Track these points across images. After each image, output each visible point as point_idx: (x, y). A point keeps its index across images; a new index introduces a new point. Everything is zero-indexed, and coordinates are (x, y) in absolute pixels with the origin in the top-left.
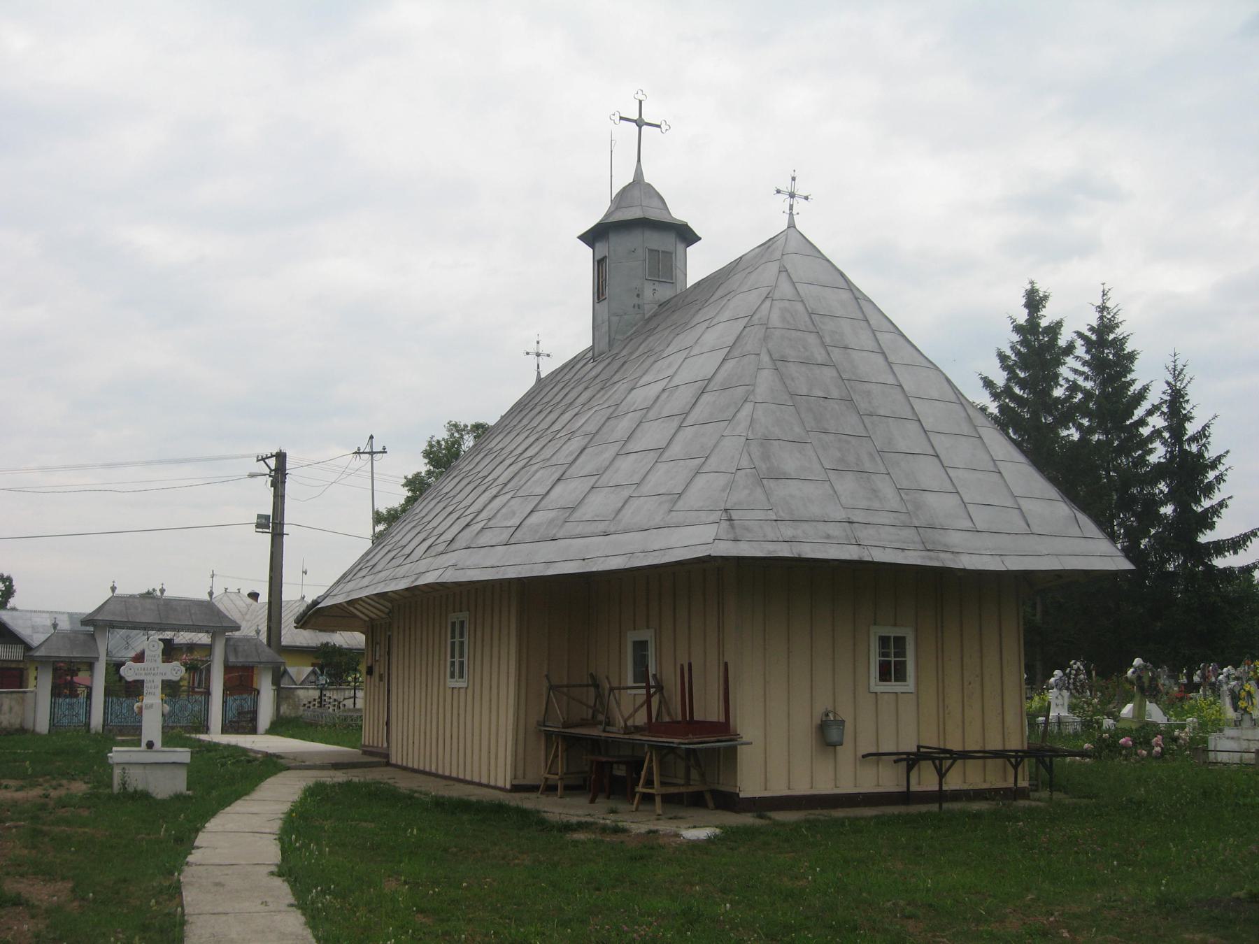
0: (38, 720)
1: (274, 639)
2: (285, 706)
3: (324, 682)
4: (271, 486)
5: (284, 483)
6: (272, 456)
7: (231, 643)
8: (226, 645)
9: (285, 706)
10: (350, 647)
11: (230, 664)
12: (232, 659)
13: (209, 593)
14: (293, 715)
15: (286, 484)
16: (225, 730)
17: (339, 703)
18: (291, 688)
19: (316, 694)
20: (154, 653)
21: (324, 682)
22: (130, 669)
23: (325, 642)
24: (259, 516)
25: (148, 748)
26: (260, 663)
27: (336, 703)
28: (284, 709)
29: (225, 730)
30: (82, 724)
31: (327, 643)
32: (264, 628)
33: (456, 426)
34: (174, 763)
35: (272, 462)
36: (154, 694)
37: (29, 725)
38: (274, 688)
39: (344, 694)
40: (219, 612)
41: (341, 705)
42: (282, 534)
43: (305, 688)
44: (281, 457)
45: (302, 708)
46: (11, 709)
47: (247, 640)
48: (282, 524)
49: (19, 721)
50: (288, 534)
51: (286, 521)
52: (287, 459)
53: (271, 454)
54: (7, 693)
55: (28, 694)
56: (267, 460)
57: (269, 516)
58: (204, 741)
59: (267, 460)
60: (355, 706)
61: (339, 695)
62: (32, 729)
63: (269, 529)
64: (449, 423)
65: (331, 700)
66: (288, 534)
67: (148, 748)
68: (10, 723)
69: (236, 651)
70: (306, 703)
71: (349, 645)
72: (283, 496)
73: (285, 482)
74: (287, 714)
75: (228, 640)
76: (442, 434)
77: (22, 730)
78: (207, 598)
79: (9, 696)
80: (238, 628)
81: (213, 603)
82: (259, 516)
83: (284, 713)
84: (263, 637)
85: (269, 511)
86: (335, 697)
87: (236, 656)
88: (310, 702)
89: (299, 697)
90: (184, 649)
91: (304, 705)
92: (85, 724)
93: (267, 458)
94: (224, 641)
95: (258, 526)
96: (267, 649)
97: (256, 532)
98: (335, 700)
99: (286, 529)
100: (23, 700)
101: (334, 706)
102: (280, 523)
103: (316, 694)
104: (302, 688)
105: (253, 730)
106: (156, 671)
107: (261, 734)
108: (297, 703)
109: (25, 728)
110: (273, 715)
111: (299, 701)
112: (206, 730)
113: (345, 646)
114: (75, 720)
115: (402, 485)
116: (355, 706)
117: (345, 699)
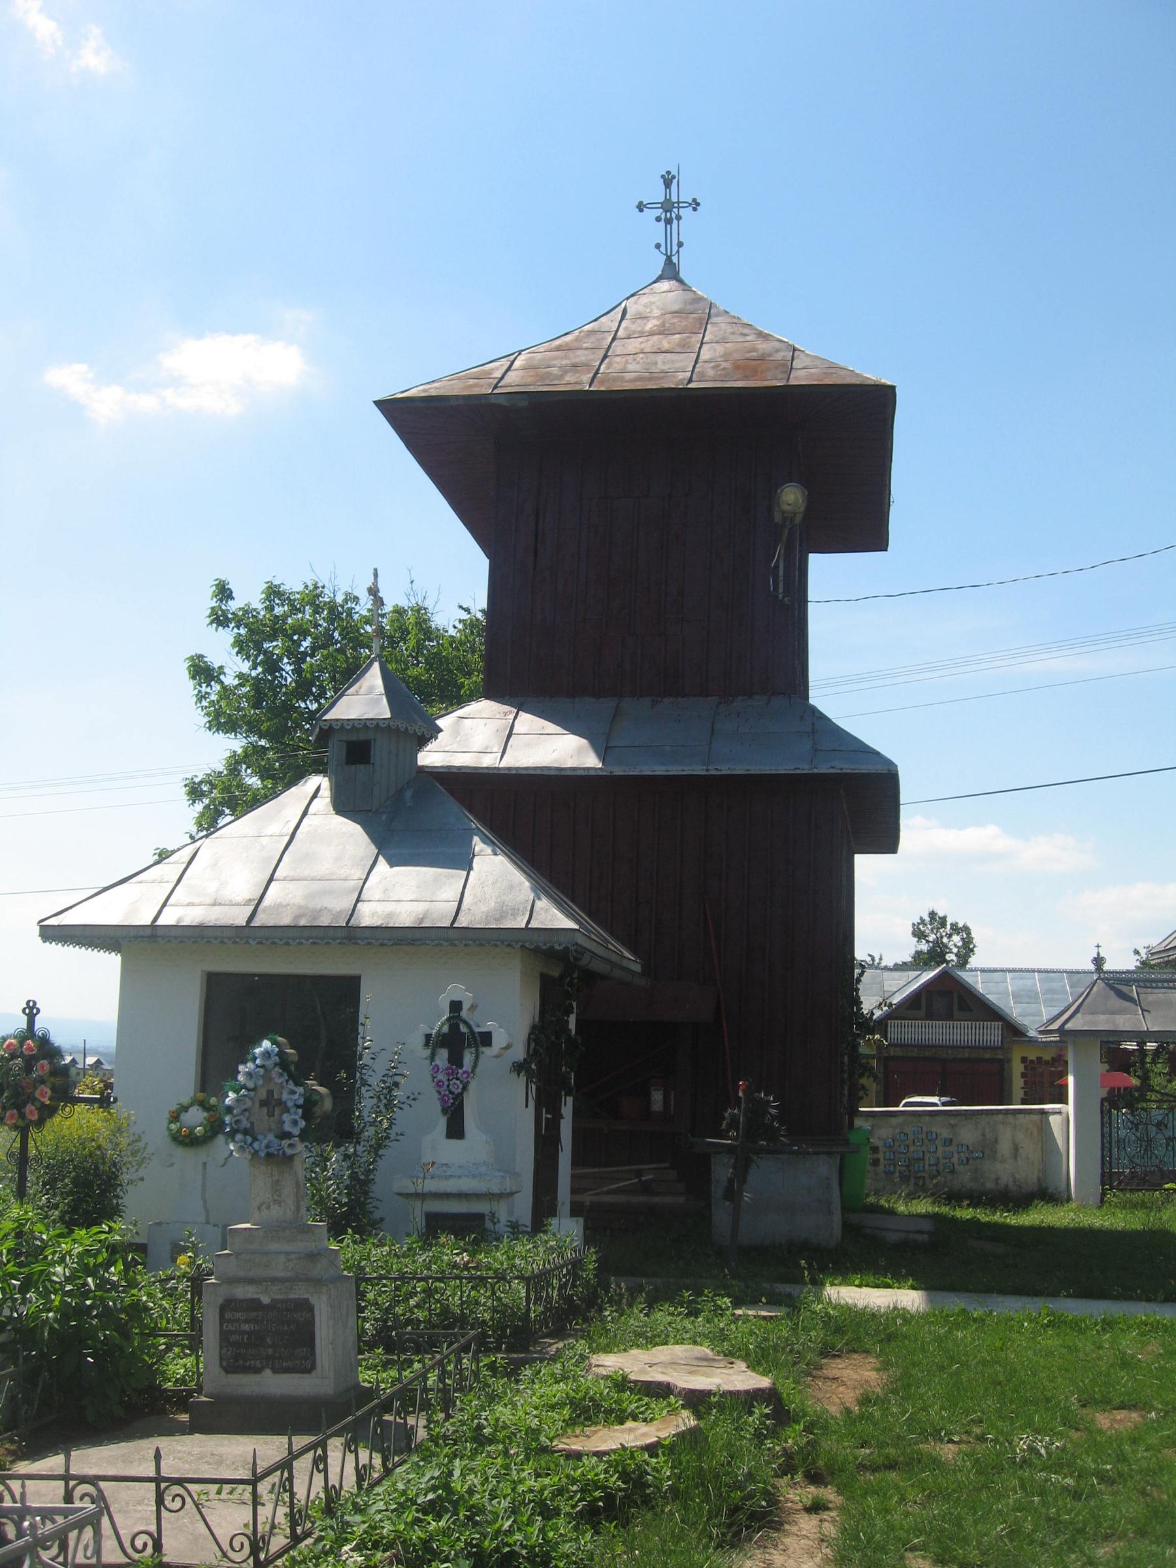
68: (1015, 1181)
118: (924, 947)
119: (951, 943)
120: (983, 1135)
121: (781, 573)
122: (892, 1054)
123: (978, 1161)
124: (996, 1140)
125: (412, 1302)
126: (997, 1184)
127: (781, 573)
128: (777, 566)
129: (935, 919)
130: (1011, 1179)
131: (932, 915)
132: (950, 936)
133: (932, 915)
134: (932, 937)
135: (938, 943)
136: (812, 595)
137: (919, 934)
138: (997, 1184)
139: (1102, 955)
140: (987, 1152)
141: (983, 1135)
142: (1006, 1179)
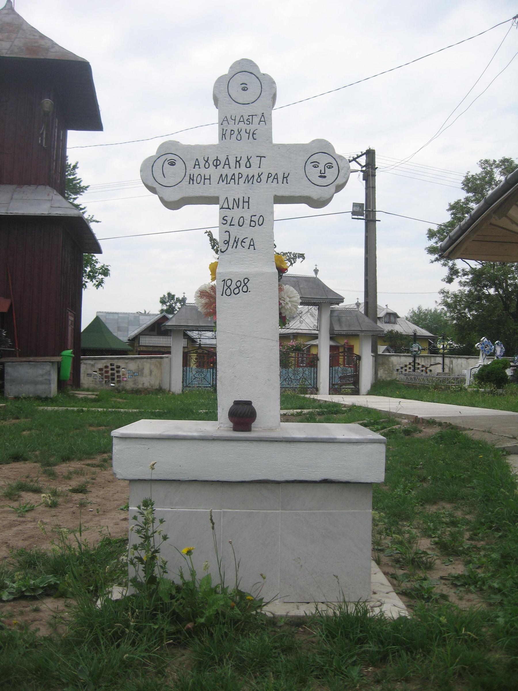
0: (173, 382)
1: (370, 311)
2: (382, 371)
3: (417, 350)
4: (363, 180)
5: (374, 175)
6: (362, 155)
7: (335, 314)
8: (331, 316)
9: (382, 371)
10: (407, 334)
11: (336, 332)
12: (337, 328)
13: (314, 270)
14: (389, 379)
15: (376, 177)
16: (334, 390)
17: (426, 368)
18: (386, 355)
19: (411, 360)
20: (246, 111)
21: (417, 350)
22: (172, 164)
23: (390, 329)
24: (355, 205)
25: (236, 428)
26: (362, 331)
27: (424, 369)
28: (381, 373)
29: (334, 390)
30: (210, 385)
31: (392, 331)
32: (362, 300)
33: (487, 161)
34: (325, 482)
35: (363, 160)
36: (252, 245)
37: (166, 386)
38: (373, 354)
39: (431, 361)
40: (324, 287)
41: (428, 371)
42: (375, 221)
43: (398, 356)
44: (370, 154)
45: (395, 373)
46: (151, 372)
47: (348, 312)
48: (374, 212)
49: (157, 383)
50: (379, 221)
51: (377, 209)
52: (376, 156)
53: (362, 152)
54: (147, 358)
55: (165, 359)
56: (357, 160)
57: (363, 204)
58: (319, 401)
59: (357, 160)
60: (443, 371)
61: (426, 362)
62: (168, 390)
63: (363, 216)
64: (480, 162)
65: (420, 366)
66: (379, 221)
67: (236, 428)
68: (150, 384)
69: (339, 321)
70: (399, 368)
71: (406, 332)
72: (374, 188)
73: (375, 176)
74: (383, 378)
75: (332, 311)
76: (477, 170)
77: (160, 390)
78: (313, 275)
79: (149, 360)
80: (341, 300)
81: (318, 279)
82: (355, 205)
83: (381, 377)
84: (362, 309)
85: (362, 200)
86: (423, 363)
87: (340, 325)
88: (402, 368)
89: (392, 363)
90: (291, 337)
91: (398, 370)
92: (213, 386)
93: (358, 157)
94: (329, 313)
95: (354, 213)
96: (366, 319)
97: (353, 218)
98: (423, 366)
99: (378, 216)
100: (161, 364)
101: (422, 371)
102: (372, 211)
103: (411, 360)
104: (396, 356)
105: (356, 392)
106: (254, 171)
107: (363, 395)
108: (391, 368)
109: (163, 388)
110: (373, 379)
111: (393, 367)
112: (316, 390)
113: (404, 333)
114: (205, 382)
115: (447, 210)
116: (443, 371)
117: (431, 365)
118: (165, 307)
119: (176, 306)
120: (138, 367)
121: (44, 136)
122: (142, 349)
123: (136, 377)
124: (143, 369)
125: (71, 561)
126: (143, 385)
127: (44, 136)
128: (42, 133)
129: (171, 296)
130: (149, 384)
131: (169, 294)
132: (176, 303)
133: (169, 294)
134: (168, 304)
135: (170, 306)
136: (68, 145)
137: (163, 302)
138: (143, 385)
139: (185, 296)
140: (140, 373)
141: (138, 367)
142: (147, 385)
